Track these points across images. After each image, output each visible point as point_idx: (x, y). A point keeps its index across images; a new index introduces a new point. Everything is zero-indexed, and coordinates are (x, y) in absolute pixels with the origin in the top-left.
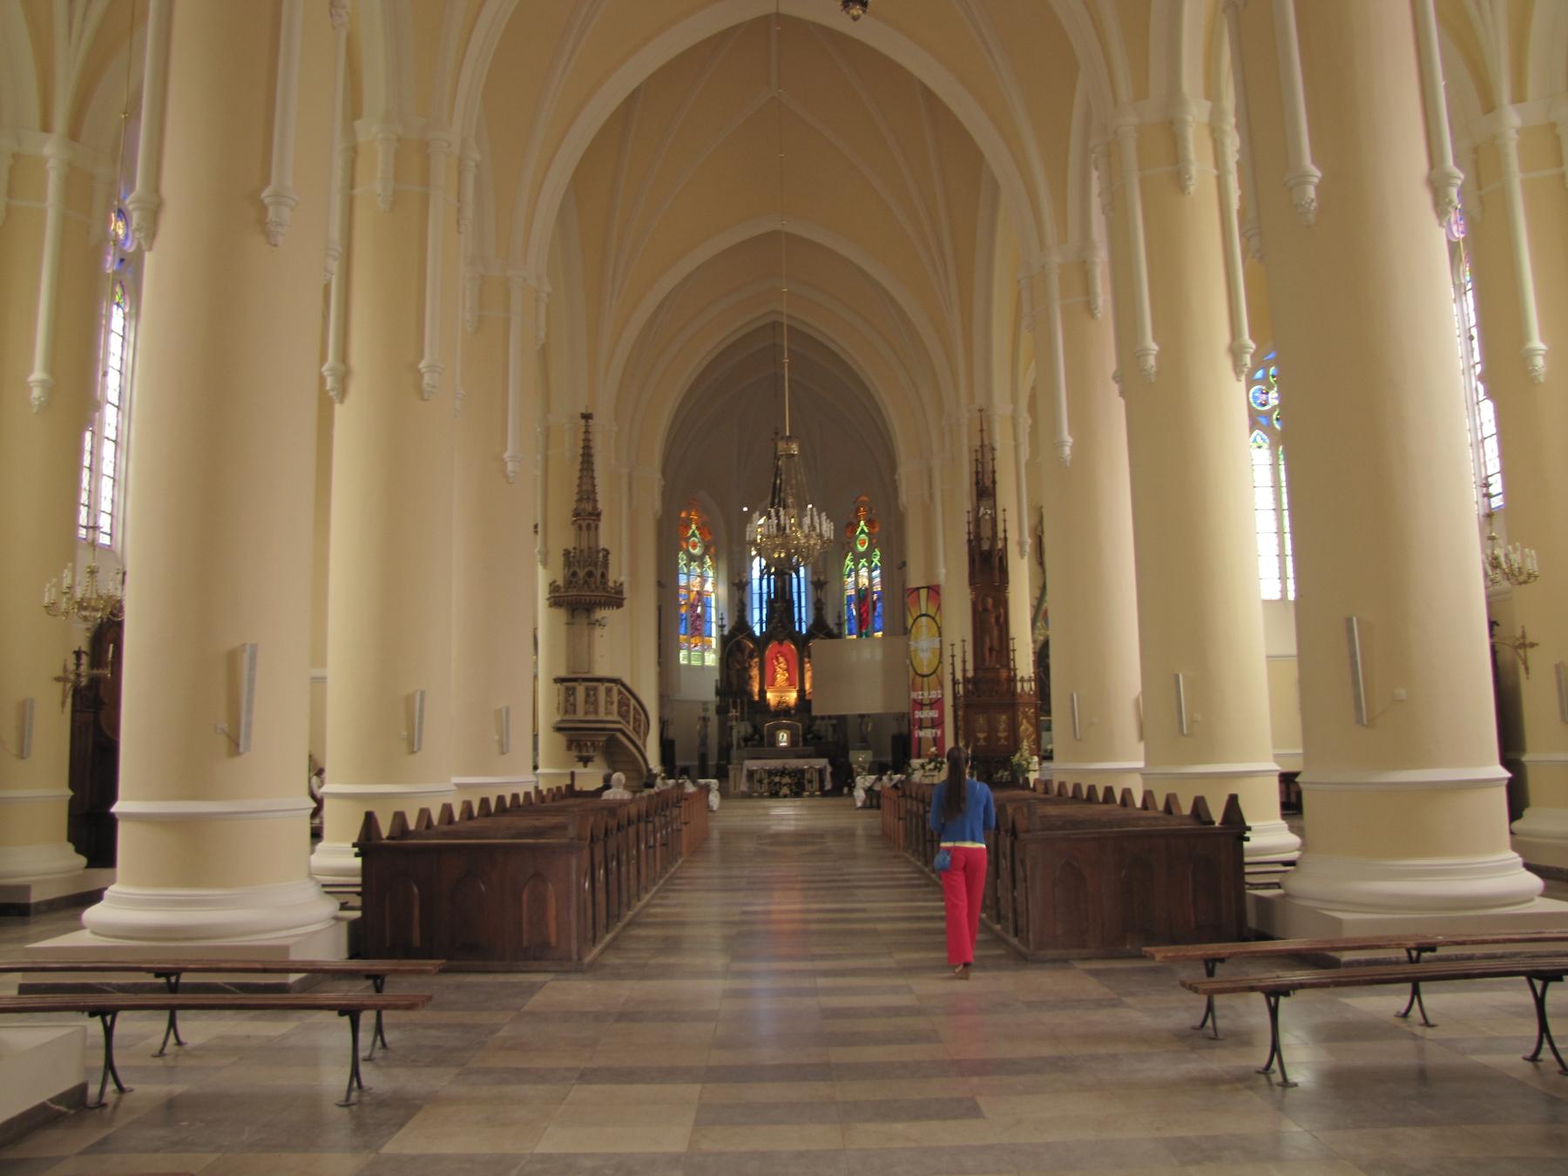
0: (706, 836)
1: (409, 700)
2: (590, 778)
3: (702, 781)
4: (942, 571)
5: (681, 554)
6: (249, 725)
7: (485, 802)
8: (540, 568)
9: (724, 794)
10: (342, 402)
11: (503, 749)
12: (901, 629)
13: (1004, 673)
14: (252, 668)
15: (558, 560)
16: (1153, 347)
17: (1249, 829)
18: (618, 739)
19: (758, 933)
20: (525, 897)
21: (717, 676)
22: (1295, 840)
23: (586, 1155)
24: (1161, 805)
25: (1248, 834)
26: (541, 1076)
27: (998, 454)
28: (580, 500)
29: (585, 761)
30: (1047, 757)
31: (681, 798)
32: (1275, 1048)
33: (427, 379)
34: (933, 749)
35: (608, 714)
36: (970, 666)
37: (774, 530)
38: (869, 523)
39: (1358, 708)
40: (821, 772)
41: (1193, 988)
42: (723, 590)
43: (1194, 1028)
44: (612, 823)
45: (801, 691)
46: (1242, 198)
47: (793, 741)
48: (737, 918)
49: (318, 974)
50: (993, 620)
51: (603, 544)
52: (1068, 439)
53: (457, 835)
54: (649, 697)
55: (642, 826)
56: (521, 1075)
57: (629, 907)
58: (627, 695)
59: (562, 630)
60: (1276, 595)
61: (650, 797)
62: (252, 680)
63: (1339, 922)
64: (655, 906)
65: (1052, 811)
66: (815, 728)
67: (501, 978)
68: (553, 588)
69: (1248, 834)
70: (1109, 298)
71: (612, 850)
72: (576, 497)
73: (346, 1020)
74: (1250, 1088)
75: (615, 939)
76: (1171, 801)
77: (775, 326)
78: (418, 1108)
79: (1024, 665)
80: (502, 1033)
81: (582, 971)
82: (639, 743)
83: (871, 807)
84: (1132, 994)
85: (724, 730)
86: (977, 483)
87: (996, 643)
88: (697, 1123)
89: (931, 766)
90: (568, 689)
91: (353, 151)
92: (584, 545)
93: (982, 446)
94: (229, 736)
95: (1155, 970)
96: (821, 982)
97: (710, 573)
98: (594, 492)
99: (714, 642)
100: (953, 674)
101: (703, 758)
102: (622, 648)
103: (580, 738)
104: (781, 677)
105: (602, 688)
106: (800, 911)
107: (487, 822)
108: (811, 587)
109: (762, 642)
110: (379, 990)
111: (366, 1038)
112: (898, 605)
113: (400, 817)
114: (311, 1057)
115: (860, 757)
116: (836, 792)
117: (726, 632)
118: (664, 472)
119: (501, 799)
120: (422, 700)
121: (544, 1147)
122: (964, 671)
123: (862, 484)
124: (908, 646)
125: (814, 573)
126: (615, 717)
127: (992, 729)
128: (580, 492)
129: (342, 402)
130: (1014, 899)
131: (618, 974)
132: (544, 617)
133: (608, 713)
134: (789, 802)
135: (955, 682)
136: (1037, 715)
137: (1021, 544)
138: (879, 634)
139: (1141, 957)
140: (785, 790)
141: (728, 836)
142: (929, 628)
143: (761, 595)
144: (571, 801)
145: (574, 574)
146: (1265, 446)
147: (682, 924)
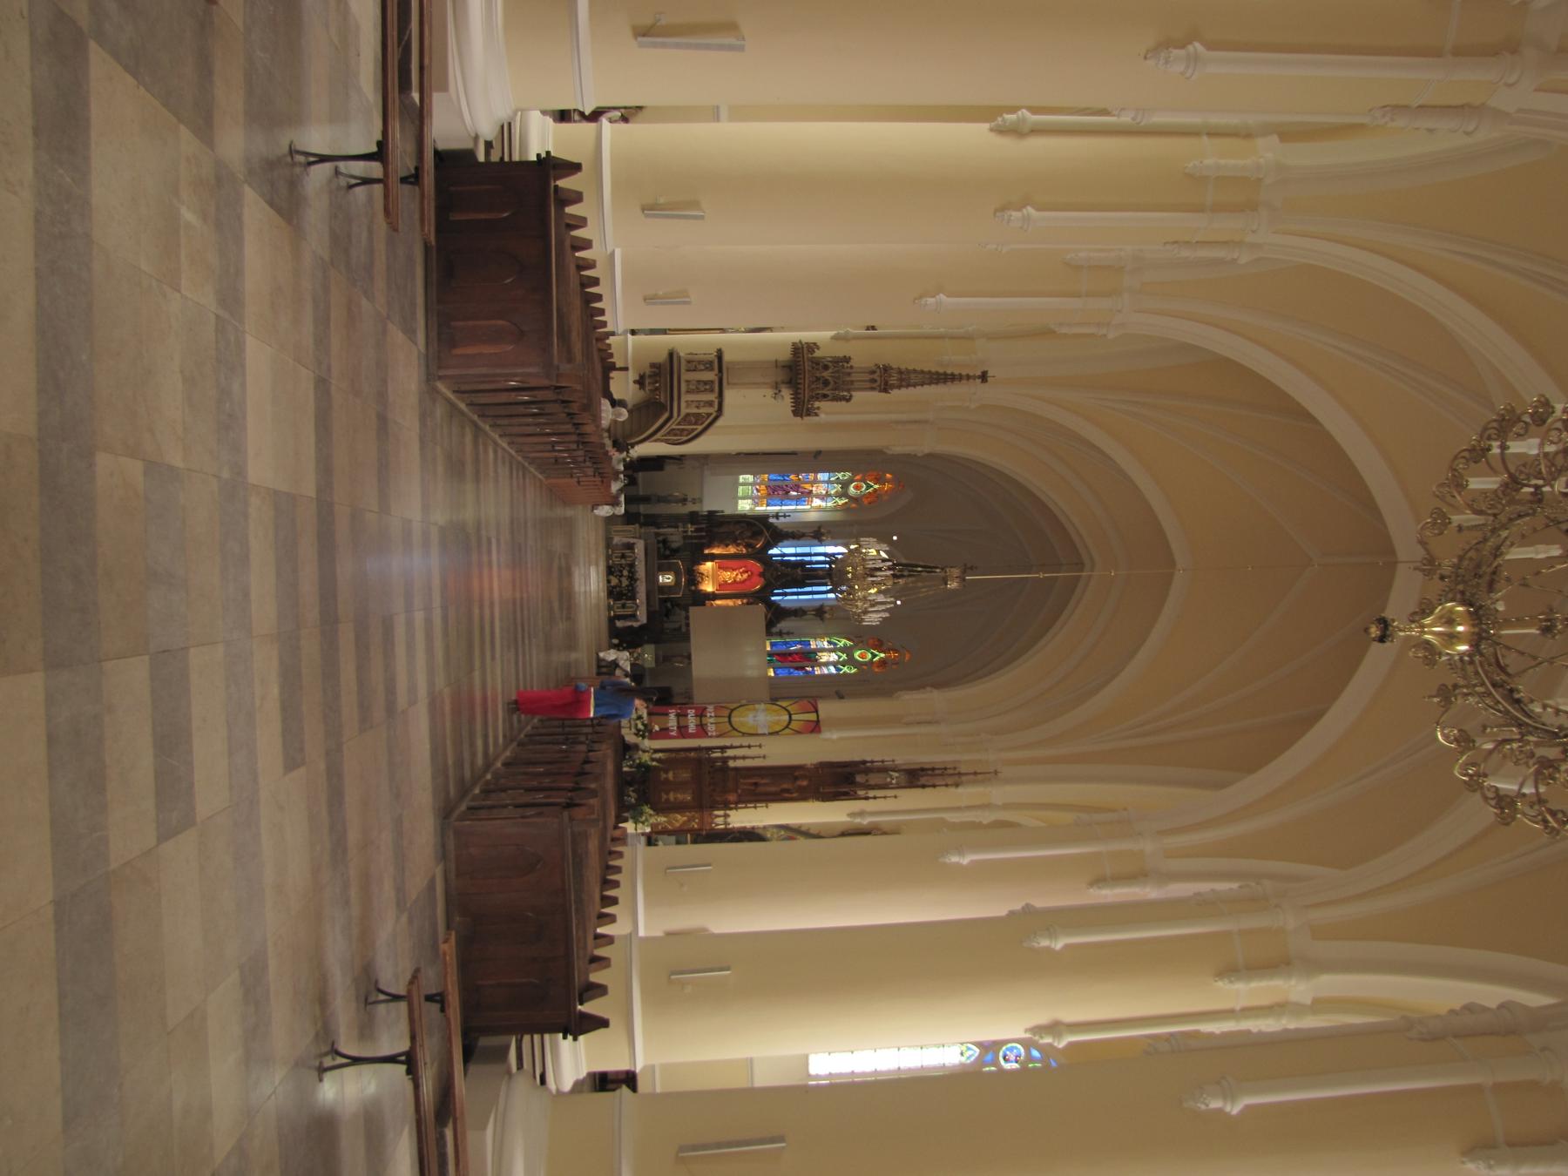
0: (567, 502)
1: (695, 204)
2: (623, 386)
3: (622, 498)
4: (835, 735)
5: (848, 474)
6: (664, 45)
7: (595, 282)
8: (833, 333)
9: (610, 520)
10: (991, 130)
11: (649, 299)
12: (776, 694)
13: (732, 797)
14: (721, 47)
15: (840, 351)
16: (1058, 945)
17: (575, 1039)
18: (657, 417)
19: (460, 554)
20: (500, 322)
21: (728, 512)
22: (567, 1085)
23: (243, 385)
24: (599, 952)
25: (570, 1038)
26: (321, 341)
27: (952, 790)
28: (900, 372)
29: (640, 382)
30: (650, 841)
31: (605, 476)
32: (356, 1061)
33: (1015, 214)
34: (657, 728)
35: (688, 403)
36: (740, 763)
37: (870, 565)
38: (883, 662)
39: (695, 1148)
40: (633, 616)
41: (415, 977)
42: (813, 517)
43: (376, 982)
44: (575, 408)
45: (714, 596)
46: (1211, 1035)
47: (663, 589)
48: (483, 533)
49: (419, 117)
50: (785, 786)
51: (857, 395)
53: (560, 254)
54: (705, 444)
55: (574, 438)
56: (322, 321)
57: (493, 426)
58: (704, 423)
60: (813, 1071)
61: (603, 446)
62: (708, 47)
63: (484, 1128)
64: (495, 452)
65: (593, 845)
66: (677, 610)
67: (420, 300)
68: (812, 347)
69: (570, 1038)
70: (1109, 900)
71: (549, 408)
72: (903, 367)
73: (374, 149)
74: (317, 1035)
75: (462, 413)
76: (602, 962)
77: (1080, 565)
78: (289, 221)
79: (741, 818)
80: (364, 302)
81: (428, 380)
82: (658, 436)
83: (599, 667)
84: (410, 921)
85: (674, 521)
86: (923, 770)
87: (761, 789)
88: (276, 492)
89: (640, 727)
90: (711, 363)
91: (1246, 134)
92: (854, 377)
93: (960, 774)
94: (653, 26)
95: (435, 946)
96: (419, 616)
97: (830, 504)
98: (908, 386)
99: (762, 509)
100: (731, 747)
101: (646, 500)
102: (752, 416)
103: (663, 376)
104: (728, 576)
105: (713, 397)
106: (491, 598)
107: (574, 283)
108: (817, 604)
109: (761, 556)
110: (404, 180)
111: (359, 168)
112: (802, 693)
113: (577, 198)
114: (338, 116)
115: (648, 655)
116: (614, 632)
117: (771, 520)
118: (930, 456)
119: (599, 298)
120: (695, 217)
121: (251, 343)
122: (735, 758)
123: (918, 654)
124: (760, 702)
125: (832, 608)
126: (684, 411)
127: (678, 786)
128: (908, 372)
129: (991, 130)
130: (505, 806)
131: (424, 416)
132: (783, 339)
133: (688, 403)
134: (603, 585)
135: (723, 749)
136: (691, 831)
137: (862, 814)
138: (771, 673)
139: (448, 927)
140: (614, 581)
141: (568, 526)
142: (777, 723)
143: (810, 555)
144: (598, 368)
146: (963, 1059)
147: (477, 479)
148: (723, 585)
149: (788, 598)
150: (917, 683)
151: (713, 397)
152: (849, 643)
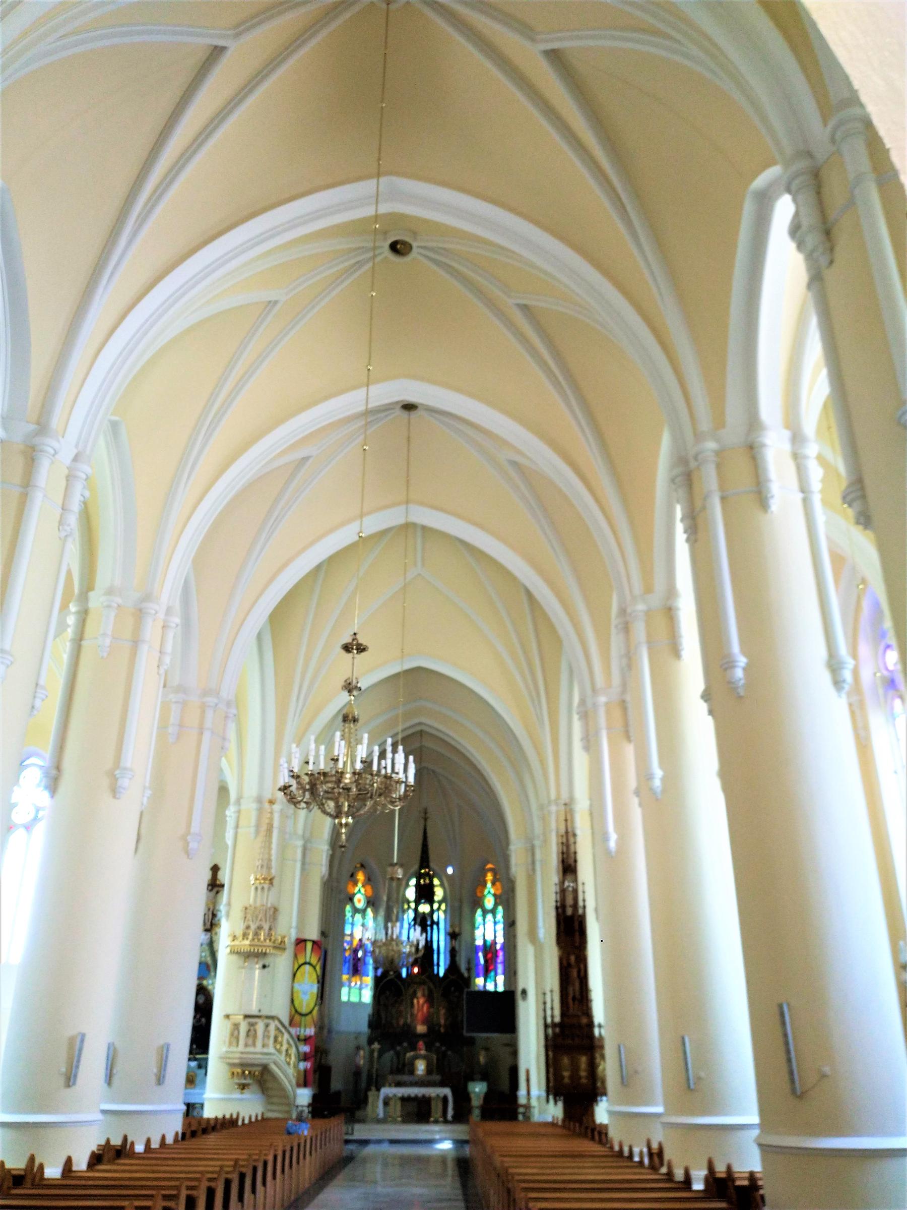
11: (160, 1079)
21: (369, 1010)
36: (557, 1012)
40: (445, 1099)
47: (429, 1071)
86: (563, 861)
87: (577, 994)
93: (567, 832)
122: (552, 1017)
125: (451, 926)
126: (271, 1050)
127: (575, 1069)
145: (248, 927)
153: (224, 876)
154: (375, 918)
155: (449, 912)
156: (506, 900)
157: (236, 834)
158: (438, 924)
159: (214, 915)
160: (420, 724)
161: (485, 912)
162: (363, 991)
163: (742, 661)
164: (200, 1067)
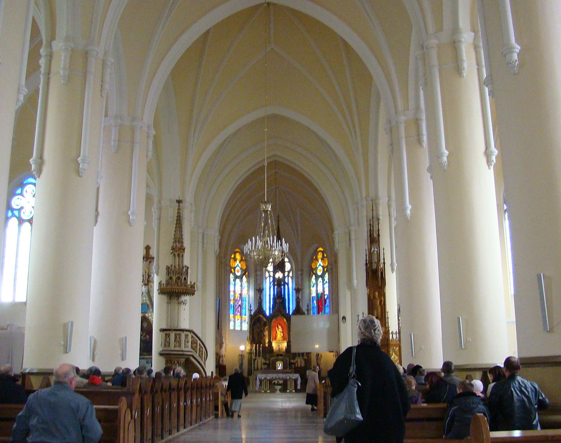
16: (446, 153)
18: (192, 363)
27: (381, 222)
28: (175, 242)
35: (186, 348)
42: (252, 293)
47: (284, 367)
50: (378, 303)
52: (409, 207)
58: (197, 342)
59: (165, 305)
72: (173, 241)
82: (202, 363)
86: (370, 236)
90: (166, 335)
99: (246, 318)
102: (193, 315)
104: (279, 335)
105: (183, 335)
108: (294, 292)
117: (252, 313)
125: (296, 285)
126: (189, 349)
129: (39, 177)
148: (284, 338)
149: (292, 307)
150: (332, 242)
151: (183, 335)
152: (314, 277)
153: (153, 253)
154: (248, 282)
155: (294, 278)
156: (332, 269)
157: (159, 224)
158: (288, 284)
159: (149, 276)
160: (275, 156)
161: (317, 277)
162: (243, 324)
163: (518, 48)
164: (147, 363)
